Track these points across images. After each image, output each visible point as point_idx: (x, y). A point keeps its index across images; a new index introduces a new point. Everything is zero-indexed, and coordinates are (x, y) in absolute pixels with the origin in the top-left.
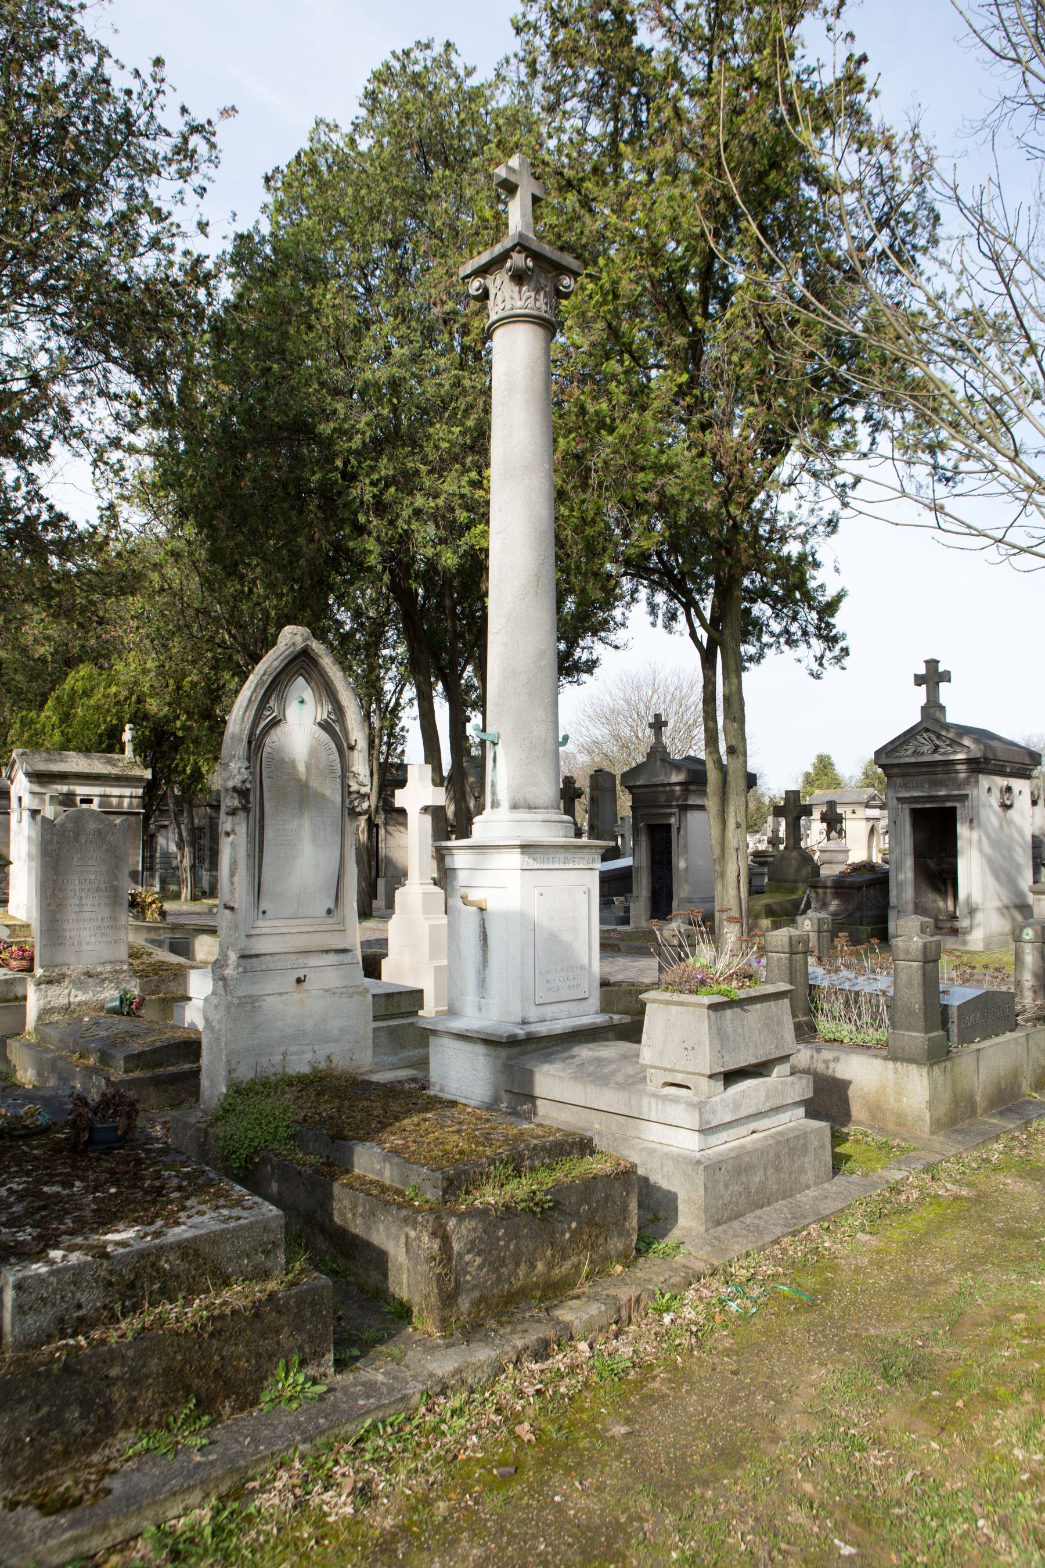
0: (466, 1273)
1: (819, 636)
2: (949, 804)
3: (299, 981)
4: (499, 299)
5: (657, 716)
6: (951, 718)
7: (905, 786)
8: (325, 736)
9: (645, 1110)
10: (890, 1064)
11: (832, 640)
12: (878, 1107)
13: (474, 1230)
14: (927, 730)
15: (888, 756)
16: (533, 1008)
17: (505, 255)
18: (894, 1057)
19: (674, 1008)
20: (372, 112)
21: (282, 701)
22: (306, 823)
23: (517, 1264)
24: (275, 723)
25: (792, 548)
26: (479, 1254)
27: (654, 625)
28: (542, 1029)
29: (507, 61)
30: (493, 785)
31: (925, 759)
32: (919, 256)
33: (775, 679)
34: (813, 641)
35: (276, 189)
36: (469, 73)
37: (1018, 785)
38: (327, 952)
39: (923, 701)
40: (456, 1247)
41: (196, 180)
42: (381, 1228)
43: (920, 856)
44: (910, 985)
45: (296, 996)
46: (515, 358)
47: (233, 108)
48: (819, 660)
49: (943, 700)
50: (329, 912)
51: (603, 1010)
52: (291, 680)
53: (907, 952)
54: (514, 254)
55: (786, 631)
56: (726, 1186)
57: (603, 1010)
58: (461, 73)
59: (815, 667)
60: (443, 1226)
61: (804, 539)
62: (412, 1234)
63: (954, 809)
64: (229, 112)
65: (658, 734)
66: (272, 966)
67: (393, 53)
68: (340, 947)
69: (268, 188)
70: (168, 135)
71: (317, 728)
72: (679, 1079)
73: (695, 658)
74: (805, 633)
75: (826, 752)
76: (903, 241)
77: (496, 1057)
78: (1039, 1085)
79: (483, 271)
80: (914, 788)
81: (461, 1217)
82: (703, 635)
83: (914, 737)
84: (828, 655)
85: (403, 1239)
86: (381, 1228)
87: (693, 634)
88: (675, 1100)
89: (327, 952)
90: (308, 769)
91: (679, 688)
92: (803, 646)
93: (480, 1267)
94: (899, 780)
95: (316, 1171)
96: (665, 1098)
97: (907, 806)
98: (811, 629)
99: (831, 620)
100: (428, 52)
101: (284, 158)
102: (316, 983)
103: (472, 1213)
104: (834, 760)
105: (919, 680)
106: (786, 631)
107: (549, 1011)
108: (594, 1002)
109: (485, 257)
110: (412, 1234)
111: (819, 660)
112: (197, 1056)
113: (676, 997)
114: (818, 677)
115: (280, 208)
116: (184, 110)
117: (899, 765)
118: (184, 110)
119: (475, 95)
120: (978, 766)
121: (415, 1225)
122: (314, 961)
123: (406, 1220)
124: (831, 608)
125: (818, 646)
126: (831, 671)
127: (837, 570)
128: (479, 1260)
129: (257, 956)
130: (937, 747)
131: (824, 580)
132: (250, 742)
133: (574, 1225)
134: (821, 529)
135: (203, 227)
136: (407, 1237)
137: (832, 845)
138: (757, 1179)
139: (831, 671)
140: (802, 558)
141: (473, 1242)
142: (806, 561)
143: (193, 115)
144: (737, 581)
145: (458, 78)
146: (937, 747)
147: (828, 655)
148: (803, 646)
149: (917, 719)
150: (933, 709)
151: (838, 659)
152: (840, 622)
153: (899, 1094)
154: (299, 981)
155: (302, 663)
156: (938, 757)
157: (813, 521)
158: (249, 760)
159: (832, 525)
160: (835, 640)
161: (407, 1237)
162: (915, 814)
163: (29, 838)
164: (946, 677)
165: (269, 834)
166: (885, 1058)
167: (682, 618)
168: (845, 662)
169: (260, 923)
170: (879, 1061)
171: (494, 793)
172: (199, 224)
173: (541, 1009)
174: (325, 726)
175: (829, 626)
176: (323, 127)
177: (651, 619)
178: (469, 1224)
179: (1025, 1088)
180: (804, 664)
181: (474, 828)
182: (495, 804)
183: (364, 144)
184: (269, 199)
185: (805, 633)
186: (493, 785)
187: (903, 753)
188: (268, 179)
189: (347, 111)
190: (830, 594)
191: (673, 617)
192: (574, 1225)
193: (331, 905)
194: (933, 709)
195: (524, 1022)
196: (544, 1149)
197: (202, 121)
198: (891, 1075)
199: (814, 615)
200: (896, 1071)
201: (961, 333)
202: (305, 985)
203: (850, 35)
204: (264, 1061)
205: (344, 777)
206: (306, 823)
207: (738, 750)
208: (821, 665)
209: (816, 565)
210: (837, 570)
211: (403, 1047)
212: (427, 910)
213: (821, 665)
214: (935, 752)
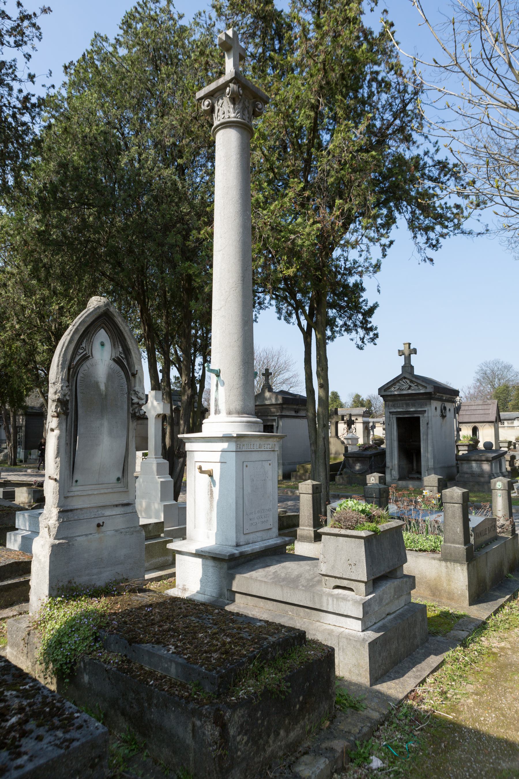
1: (362, 327)
2: (416, 415)
3: (99, 525)
5: (267, 370)
6: (416, 372)
7: (394, 406)
8: (117, 368)
9: (325, 604)
10: (443, 563)
11: (368, 330)
12: (436, 588)
13: (243, 716)
14: (405, 378)
15: (385, 391)
18: (446, 558)
19: (341, 539)
20: (126, 32)
21: (91, 342)
22: (106, 423)
23: (269, 736)
25: (351, 280)
26: (246, 734)
27: (279, 318)
29: (200, 14)
30: (216, 400)
31: (405, 392)
32: (414, 134)
33: (341, 348)
34: (359, 330)
35: (71, 74)
36: (181, 17)
37: (448, 405)
38: (117, 506)
39: (403, 363)
40: (232, 732)
41: (26, 49)
42: (172, 716)
43: (401, 440)
44: (454, 516)
45: (97, 536)
46: (227, 145)
47: (49, 9)
48: (362, 339)
49: (412, 363)
50: (118, 479)
51: (280, 535)
53: (452, 498)
55: (345, 324)
57: (280, 535)
58: (176, 17)
59: (360, 343)
60: (222, 717)
61: (361, 274)
62: (198, 723)
64: (46, 10)
65: (267, 379)
66: (81, 517)
69: (66, 73)
70: (9, 18)
71: (112, 362)
72: (345, 583)
74: (355, 325)
75: (335, 391)
76: (406, 125)
77: (221, 568)
78: (511, 570)
80: (398, 407)
81: (234, 707)
82: (304, 323)
83: (398, 382)
84: (367, 337)
86: (172, 716)
87: (299, 324)
88: (345, 599)
89: (117, 506)
90: (106, 388)
92: (354, 332)
93: (247, 743)
94: (391, 403)
97: (394, 416)
98: (358, 323)
99: (369, 319)
101: (76, 57)
103: (241, 703)
104: (339, 394)
105: (401, 353)
106: (345, 324)
107: (251, 537)
108: (275, 530)
110: (198, 723)
111: (362, 339)
113: (343, 532)
114: (361, 348)
116: (19, 4)
117: (391, 395)
118: (19, 4)
120: (429, 397)
121: (200, 716)
122: (108, 512)
123: (193, 712)
124: (371, 312)
125: (361, 332)
128: (245, 738)
129: (71, 510)
130: (410, 386)
131: (369, 297)
132: (69, 369)
133: (301, 698)
135: (31, 77)
136: (194, 726)
137: (350, 435)
138: (394, 646)
140: (356, 285)
141: (242, 725)
142: (359, 288)
143: (25, 8)
144: (324, 297)
146: (410, 386)
147: (367, 337)
148: (354, 332)
149: (400, 372)
150: (408, 368)
151: (372, 340)
152: (374, 320)
153: (449, 580)
154: (99, 525)
155: (103, 319)
156: (410, 392)
157: (367, 264)
158: (68, 381)
159: (377, 267)
160: (371, 329)
161: (194, 726)
163: (508, 368)
164: (415, 351)
165: (81, 429)
166: (440, 560)
167: (294, 316)
168: (376, 341)
169: (74, 489)
170: (437, 562)
171: (216, 405)
173: (247, 537)
174: (117, 361)
175: (367, 322)
176: (98, 38)
177: (278, 315)
178: (240, 712)
179: (505, 572)
180: (354, 342)
182: (217, 412)
183: (122, 52)
184: (66, 79)
185: (355, 325)
188: (66, 68)
189: (113, 31)
190: (370, 304)
191: (290, 315)
192: (301, 698)
194: (408, 368)
195: (238, 545)
196: (279, 644)
197: (31, 13)
198: (444, 570)
199: (360, 316)
200: (447, 567)
202: (103, 529)
203: (386, 11)
204: (76, 580)
205: (129, 393)
206: (106, 423)
207: (324, 386)
208: (363, 342)
209: (363, 290)
212: (159, 473)
213: (363, 342)
214: (409, 389)
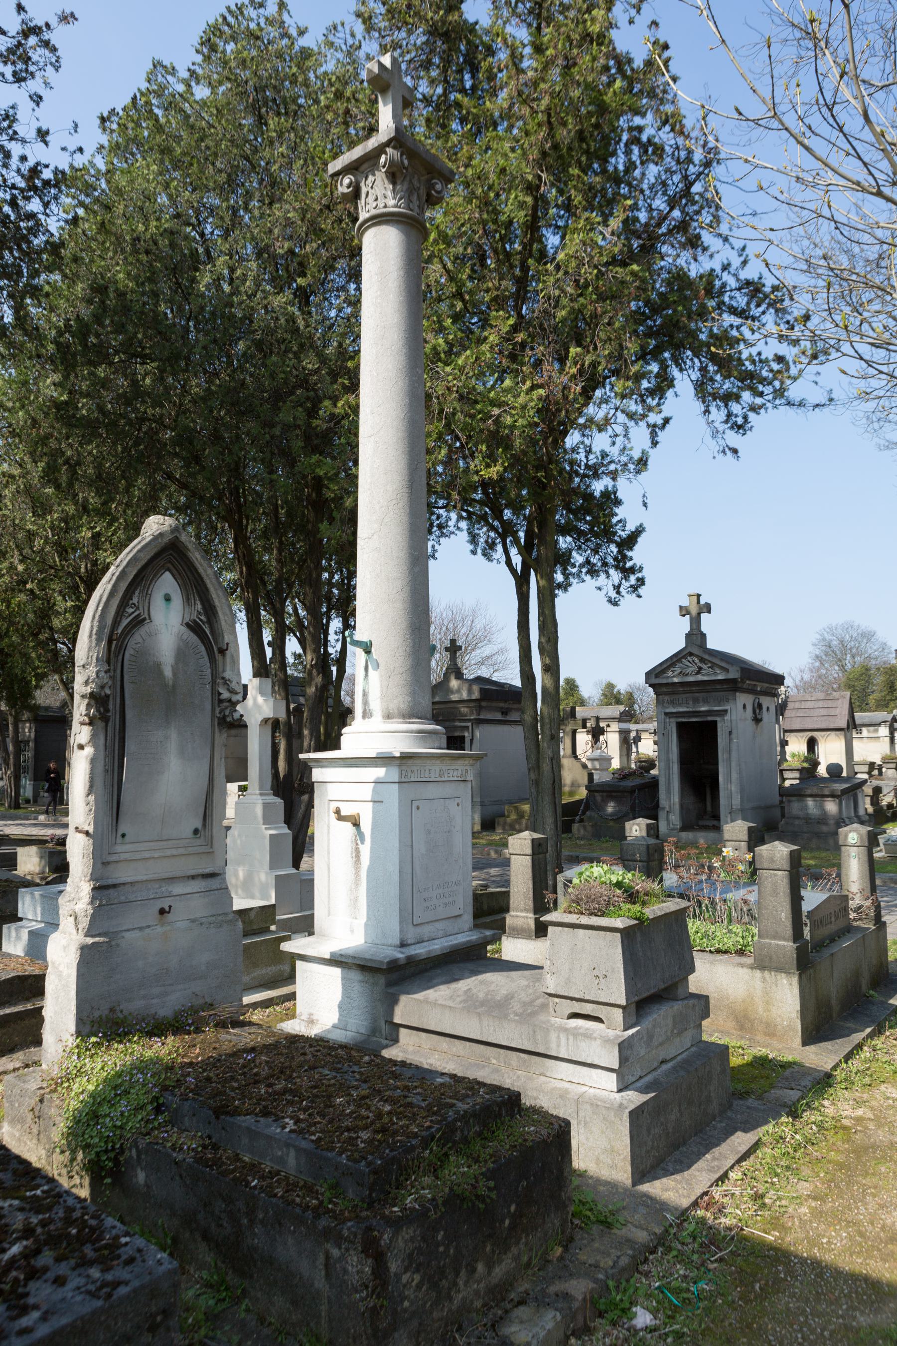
0: (403, 1298)
1: (617, 568)
2: (710, 719)
3: (162, 912)
4: (371, 198)
5: (453, 641)
7: (672, 703)
8: (194, 638)
9: (553, 1045)
10: (758, 974)
11: (627, 572)
12: (746, 1017)
13: (412, 1239)
14: (691, 654)
15: (657, 676)
16: (411, 929)
17: (380, 150)
20: (207, 58)
21: (147, 595)
24: (138, 622)
25: (598, 487)
26: (417, 1270)
27: (474, 552)
28: (420, 951)
29: (335, 28)
33: (581, 603)
34: (612, 571)
35: (112, 131)
36: (302, 32)
37: (766, 701)
38: (193, 877)
39: (687, 629)
40: (394, 1267)
41: (34, 85)
43: (684, 762)
45: (159, 929)
48: (617, 588)
49: (704, 629)
50: (196, 831)
51: (476, 926)
52: (156, 575)
53: (772, 860)
54: (389, 150)
55: (588, 562)
56: (649, 1130)
58: (293, 32)
59: (613, 594)
61: (614, 475)
62: (335, 1252)
63: (715, 722)
65: (453, 658)
66: (132, 897)
67: (228, 8)
68: (208, 871)
69: (104, 129)
72: (588, 1009)
73: (510, 583)
74: (605, 564)
75: (572, 677)
77: (374, 984)
79: (353, 168)
80: (680, 705)
81: (396, 1224)
82: (517, 560)
83: (679, 661)
85: (321, 1259)
87: (509, 562)
88: (588, 1036)
89: (193, 877)
90: (175, 674)
91: (453, 620)
92: (603, 576)
93: (419, 1287)
94: (667, 698)
95: (199, 1160)
96: (575, 1034)
98: (610, 560)
99: (629, 554)
100: (261, 11)
101: (121, 101)
102: (180, 916)
104: (579, 682)
105: (684, 611)
107: (426, 931)
109: (357, 152)
110: (335, 1252)
111: (617, 588)
112: (40, 992)
114: (615, 604)
115: (115, 148)
117: (667, 684)
119: (306, 54)
120: (732, 687)
121: (339, 1240)
124: (631, 540)
125: (616, 576)
126: (628, 599)
127: (645, 505)
128: (417, 1278)
129: (114, 886)
130: (700, 668)
131: (628, 515)
132: (110, 642)
134: (631, 467)
135: (43, 135)
136: (328, 1257)
138: (673, 1117)
139: (628, 599)
140: (606, 494)
141: (411, 1255)
142: (610, 499)
145: (289, 37)
146: (700, 668)
148: (603, 576)
150: (696, 636)
151: (635, 588)
152: (637, 555)
153: (768, 1003)
154: (162, 912)
155: (169, 555)
156: (700, 678)
157: (624, 459)
159: (642, 463)
160: (632, 570)
161: (328, 1257)
162: (680, 726)
166: (752, 967)
167: (500, 548)
168: (641, 591)
169: (119, 848)
172: (39, 131)
173: (419, 930)
174: (194, 627)
175: (625, 558)
177: (471, 547)
178: (407, 1233)
179: (864, 988)
180: (604, 592)
181: (343, 739)
182: (366, 714)
183: (201, 92)
184: (104, 140)
185: (605, 564)
186: (365, 694)
187: (670, 674)
188: (103, 120)
189: (184, 56)
190: (631, 527)
191: (492, 546)
193: (198, 824)
194: (696, 636)
195: (403, 945)
197: (40, 22)
198: (758, 984)
200: (764, 980)
201: (741, 301)
202: (170, 917)
205: (214, 683)
206: (174, 735)
207: (552, 668)
208: (618, 593)
209: (618, 502)
210: (645, 505)
211: (255, 965)
213: (618, 593)
214: (698, 673)
